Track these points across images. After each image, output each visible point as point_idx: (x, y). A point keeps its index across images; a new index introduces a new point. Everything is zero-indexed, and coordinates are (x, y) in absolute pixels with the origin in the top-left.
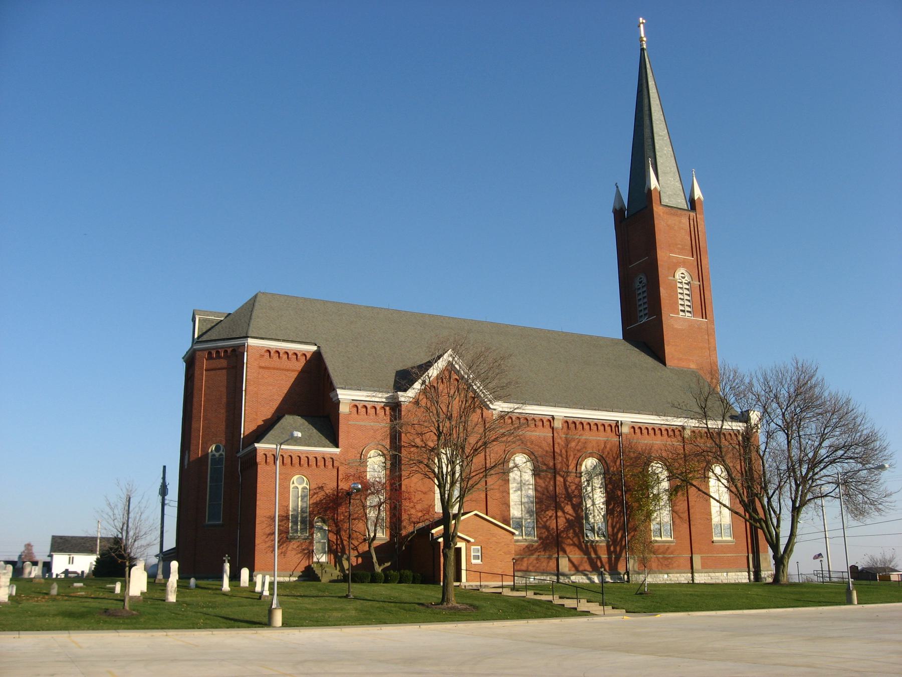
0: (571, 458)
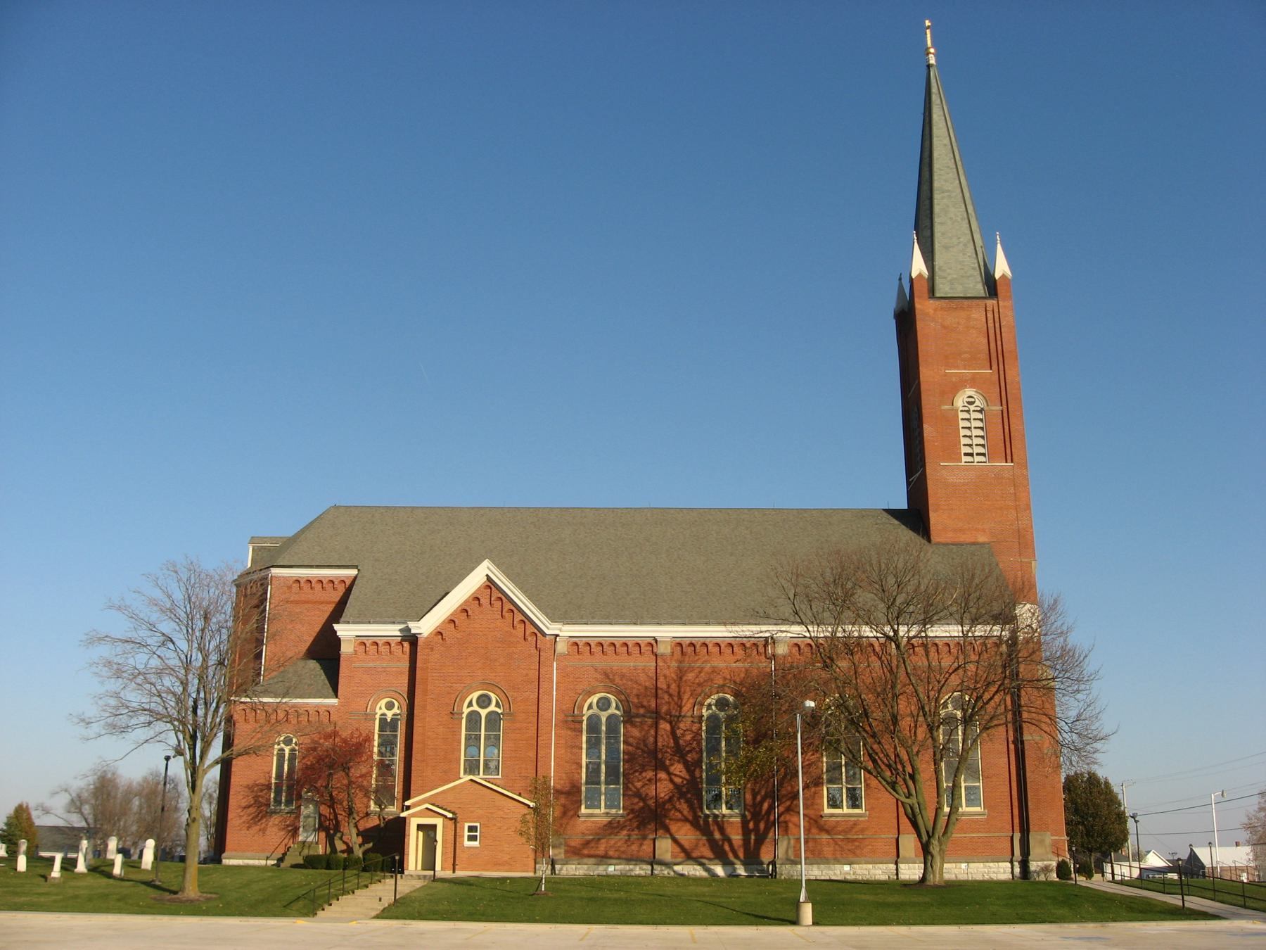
0: (686, 697)
